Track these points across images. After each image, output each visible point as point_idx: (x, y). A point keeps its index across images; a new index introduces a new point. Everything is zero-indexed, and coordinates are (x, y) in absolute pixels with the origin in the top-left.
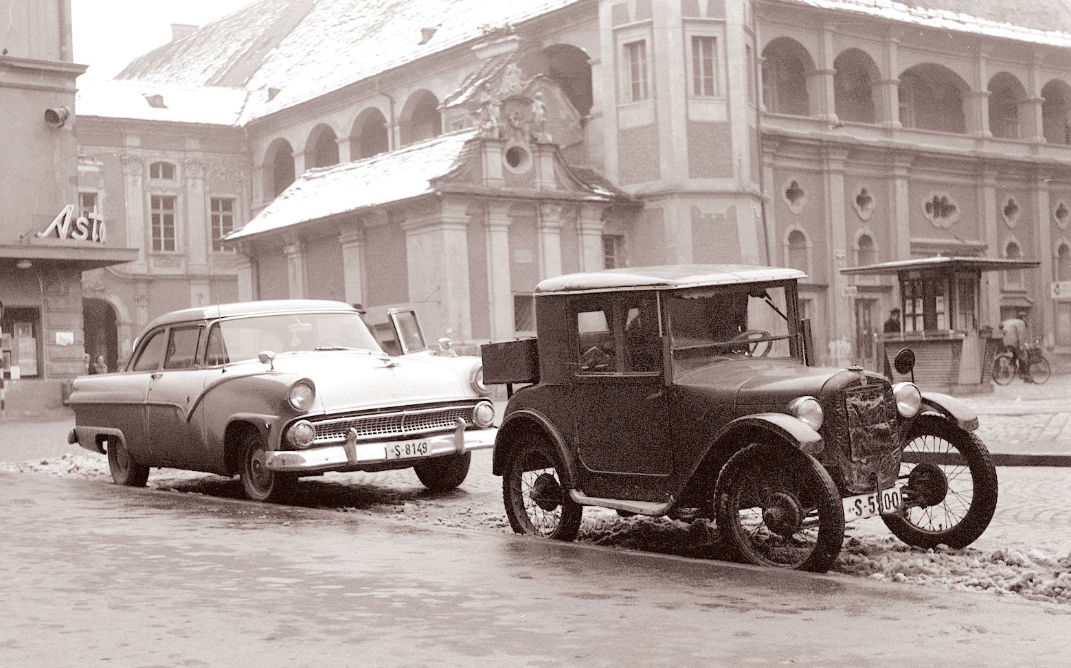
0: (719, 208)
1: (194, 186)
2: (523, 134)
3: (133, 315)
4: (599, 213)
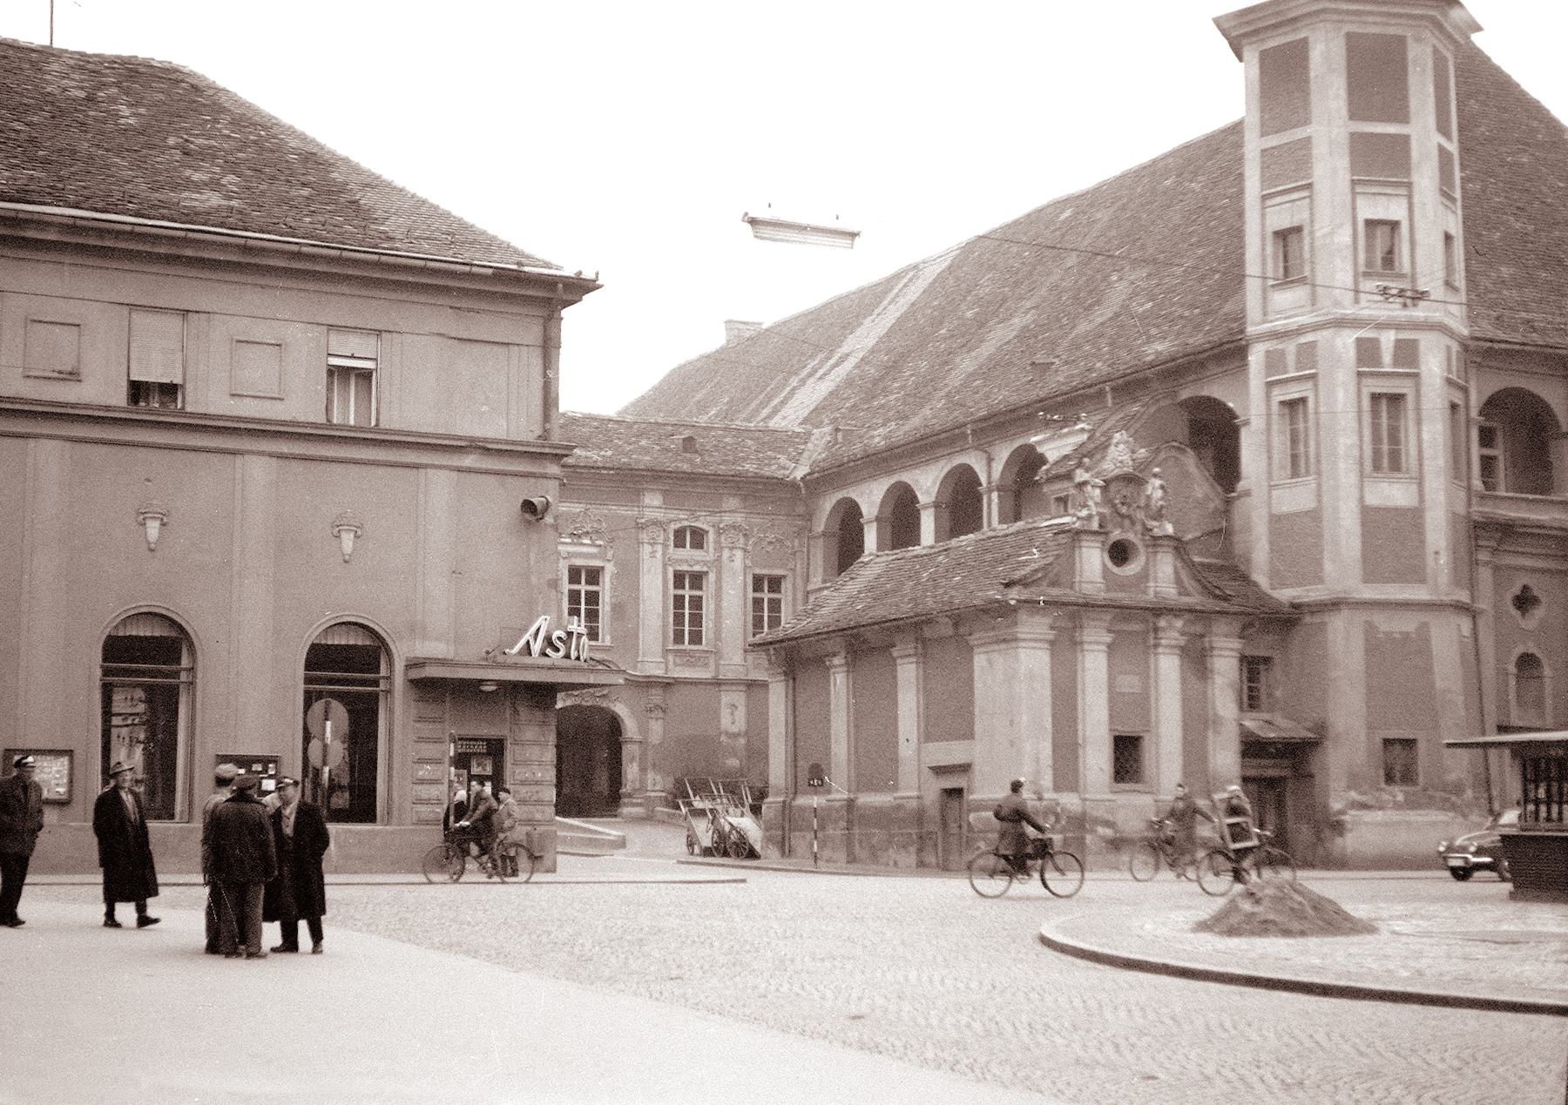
0: (1407, 624)
2: (1133, 523)
3: (643, 729)
4: (1236, 627)
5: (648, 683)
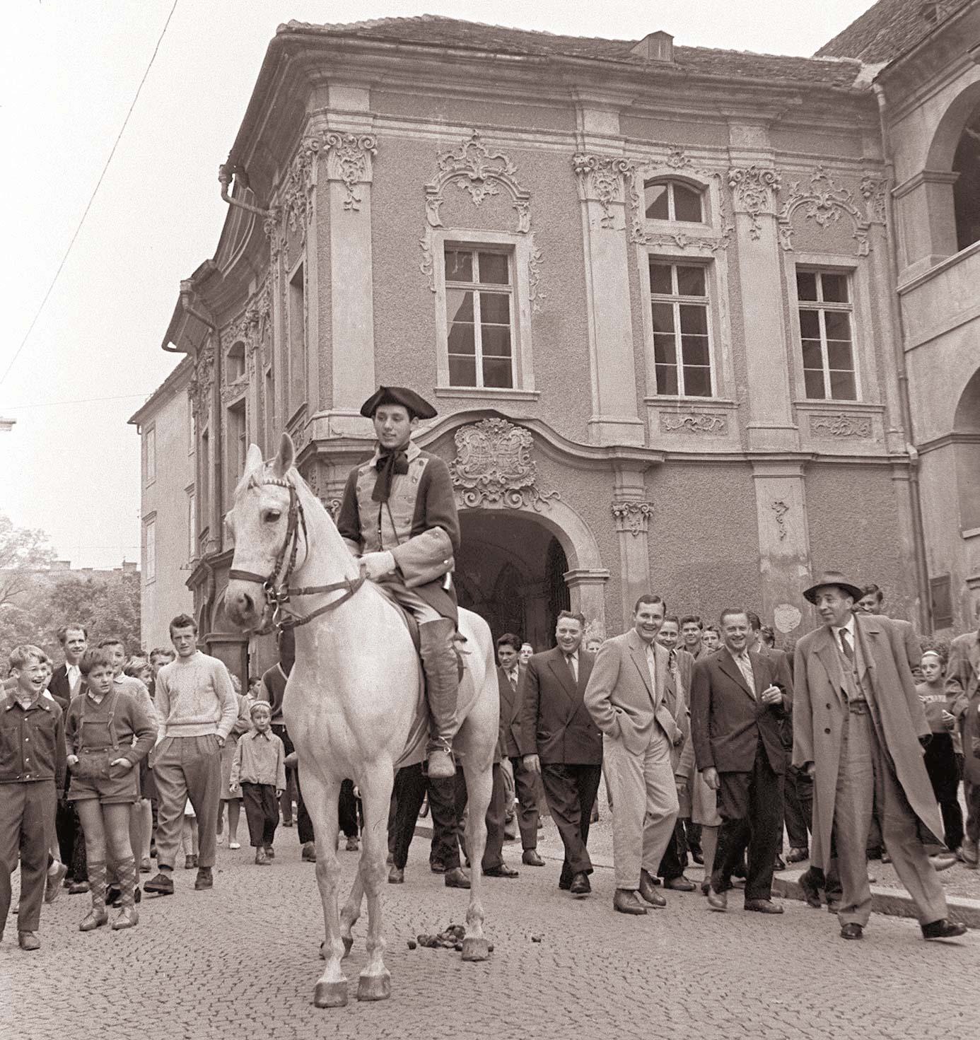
1: (754, 234)
3: (610, 554)
5: (612, 464)
